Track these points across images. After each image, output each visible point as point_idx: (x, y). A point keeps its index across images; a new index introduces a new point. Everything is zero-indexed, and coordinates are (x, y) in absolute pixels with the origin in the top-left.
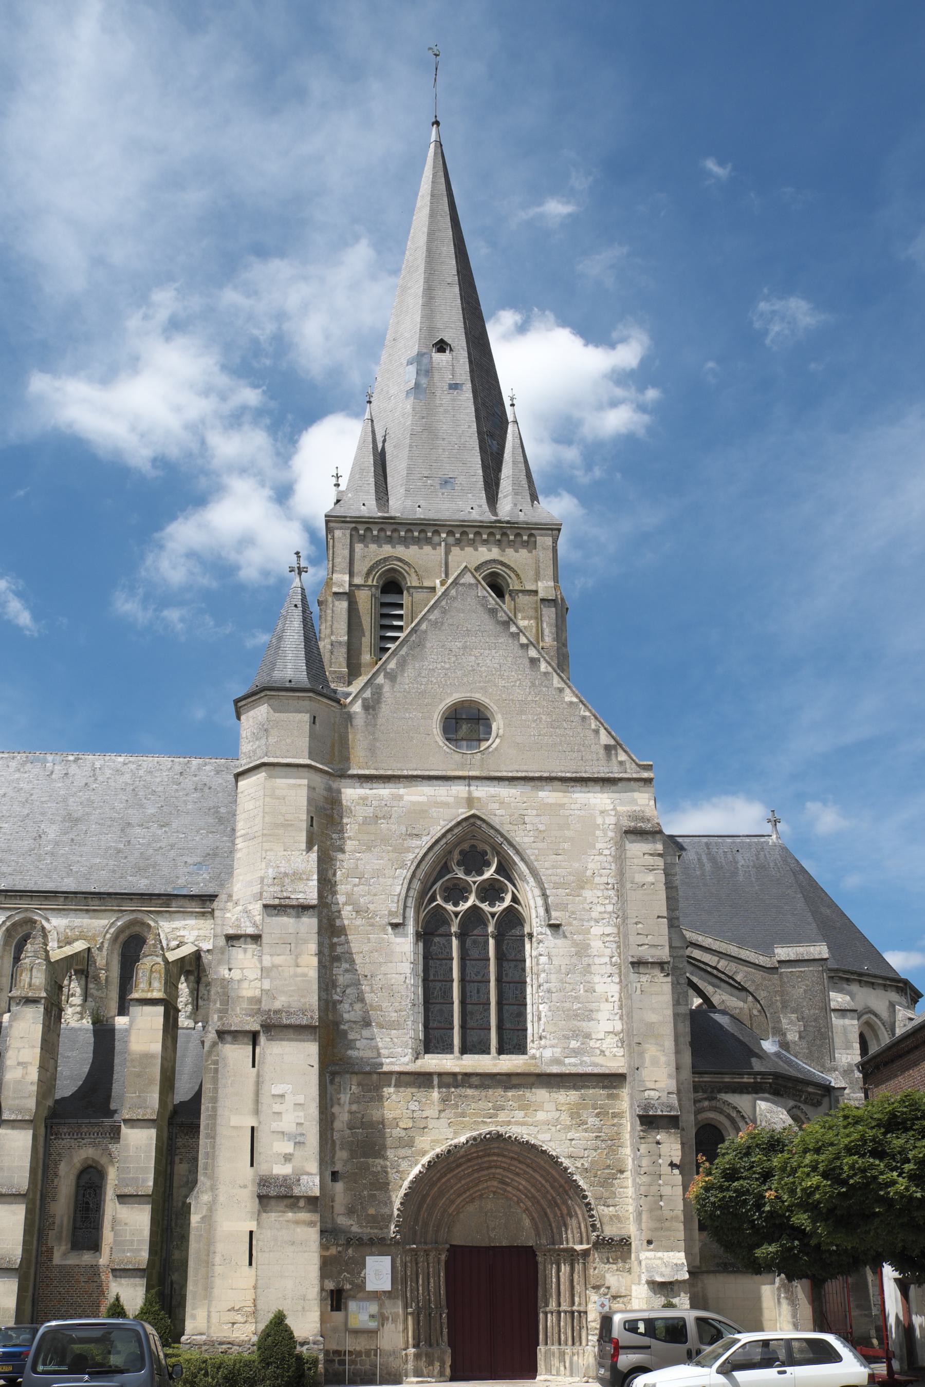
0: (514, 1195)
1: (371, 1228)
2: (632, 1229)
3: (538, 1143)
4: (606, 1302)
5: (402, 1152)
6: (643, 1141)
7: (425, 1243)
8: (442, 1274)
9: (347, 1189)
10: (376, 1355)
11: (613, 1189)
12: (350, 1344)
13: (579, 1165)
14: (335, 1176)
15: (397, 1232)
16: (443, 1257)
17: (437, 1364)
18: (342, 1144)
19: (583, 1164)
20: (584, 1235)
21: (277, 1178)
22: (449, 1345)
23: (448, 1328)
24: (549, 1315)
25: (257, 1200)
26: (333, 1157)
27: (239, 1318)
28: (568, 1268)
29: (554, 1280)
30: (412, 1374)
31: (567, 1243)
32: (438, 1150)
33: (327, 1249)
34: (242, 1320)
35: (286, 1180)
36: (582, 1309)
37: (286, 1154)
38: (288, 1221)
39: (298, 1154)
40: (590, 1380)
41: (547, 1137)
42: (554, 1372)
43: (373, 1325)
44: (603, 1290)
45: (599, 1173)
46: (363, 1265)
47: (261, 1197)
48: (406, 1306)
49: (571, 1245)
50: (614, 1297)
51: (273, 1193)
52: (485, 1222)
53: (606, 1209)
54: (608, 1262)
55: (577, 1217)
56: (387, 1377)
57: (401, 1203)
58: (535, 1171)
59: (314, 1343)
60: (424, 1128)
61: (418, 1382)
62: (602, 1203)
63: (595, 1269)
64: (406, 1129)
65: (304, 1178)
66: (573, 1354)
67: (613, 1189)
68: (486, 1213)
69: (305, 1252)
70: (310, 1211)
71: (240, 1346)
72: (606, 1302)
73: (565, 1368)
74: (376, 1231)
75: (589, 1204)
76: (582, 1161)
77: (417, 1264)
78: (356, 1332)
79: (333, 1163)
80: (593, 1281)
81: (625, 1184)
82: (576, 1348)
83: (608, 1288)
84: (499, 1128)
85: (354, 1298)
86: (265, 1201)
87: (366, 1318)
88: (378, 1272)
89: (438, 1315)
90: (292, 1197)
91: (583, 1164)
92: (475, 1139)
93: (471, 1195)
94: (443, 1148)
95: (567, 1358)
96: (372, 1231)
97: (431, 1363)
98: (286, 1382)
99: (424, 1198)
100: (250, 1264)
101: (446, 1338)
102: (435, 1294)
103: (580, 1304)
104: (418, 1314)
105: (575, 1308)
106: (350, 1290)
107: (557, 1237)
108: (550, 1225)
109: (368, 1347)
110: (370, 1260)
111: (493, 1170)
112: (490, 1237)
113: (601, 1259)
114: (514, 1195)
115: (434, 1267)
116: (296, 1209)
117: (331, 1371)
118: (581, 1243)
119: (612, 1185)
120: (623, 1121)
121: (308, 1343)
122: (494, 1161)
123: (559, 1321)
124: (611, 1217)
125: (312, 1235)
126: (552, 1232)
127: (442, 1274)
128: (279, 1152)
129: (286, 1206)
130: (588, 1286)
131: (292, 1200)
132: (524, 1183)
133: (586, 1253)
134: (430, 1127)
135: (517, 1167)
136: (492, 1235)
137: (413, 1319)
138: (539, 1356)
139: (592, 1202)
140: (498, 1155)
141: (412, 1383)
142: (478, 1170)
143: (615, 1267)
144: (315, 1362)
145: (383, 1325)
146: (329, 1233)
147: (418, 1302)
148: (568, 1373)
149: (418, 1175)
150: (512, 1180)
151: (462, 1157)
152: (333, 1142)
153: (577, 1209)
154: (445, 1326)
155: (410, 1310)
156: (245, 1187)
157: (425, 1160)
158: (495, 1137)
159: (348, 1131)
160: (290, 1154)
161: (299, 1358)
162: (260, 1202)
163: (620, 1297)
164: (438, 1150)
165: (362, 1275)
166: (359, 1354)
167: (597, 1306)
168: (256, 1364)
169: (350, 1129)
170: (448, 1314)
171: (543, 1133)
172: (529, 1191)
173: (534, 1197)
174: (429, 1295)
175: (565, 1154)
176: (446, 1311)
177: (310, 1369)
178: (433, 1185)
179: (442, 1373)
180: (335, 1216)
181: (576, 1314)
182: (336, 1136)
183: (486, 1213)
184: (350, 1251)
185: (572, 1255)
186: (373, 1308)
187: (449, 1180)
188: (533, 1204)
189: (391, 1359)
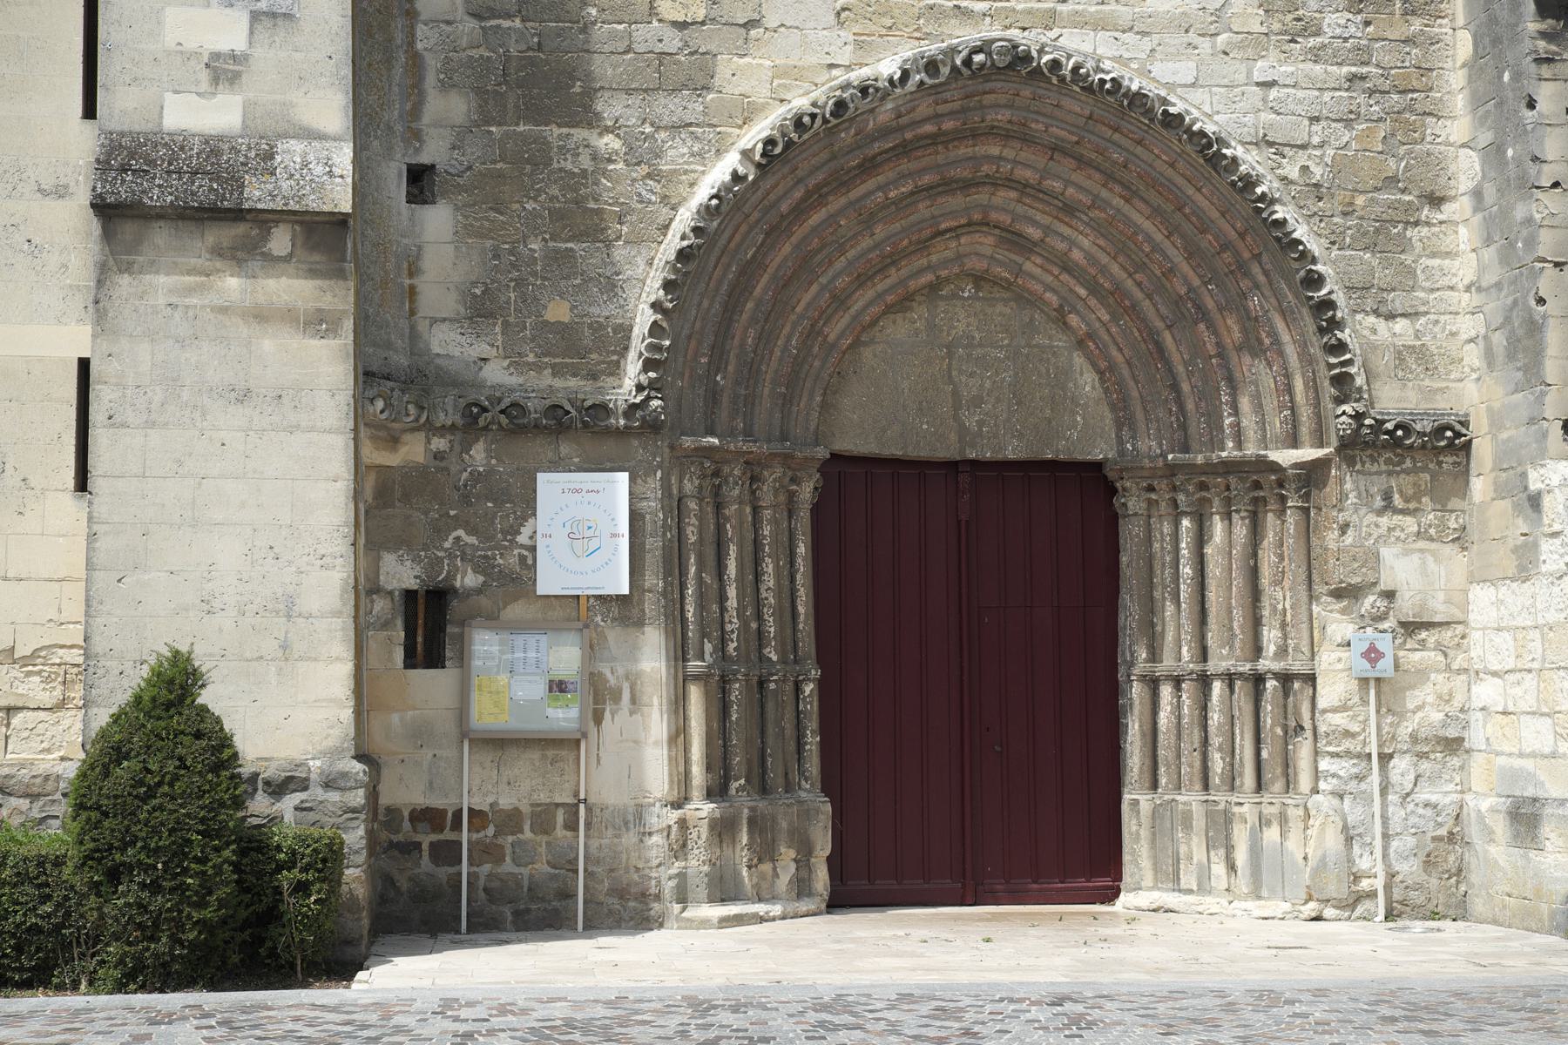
0: (1048, 288)
1: (557, 371)
2: (1472, 391)
3: (1152, 89)
4: (1385, 644)
5: (670, 107)
6: (1546, 71)
7: (748, 433)
8: (802, 549)
9: (466, 231)
10: (572, 826)
11: (1408, 258)
12: (477, 786)
13: (1293, 172)
14: (420, 182)
15: (652, 385)
16: (806, 492)
17: (787, 854)
18: (448, 68)
19: (1305, 169)
20: (1305, 414)
21: (177, 144)
22: (826, 789)
23: (823, 730)
24: (1166, 691)
25: (95, 226)
26: (416, 112)
27: (35, 690)
28: (1241, 531)
29: (1187, 571)
30: (703, 892)
31: (1239, 445)
32: (800, 103)
33: (393, 441)
34: (48, 697)
35: (215, 152)
36: (1297, 665)
37: (216, 56)
38: (224, 310)
39: (268, 57)
40: (1329, 912)
41: (1184, 71)
42: (1188, 880)
43: (564, 716)
44: (1369, 602)
45: (1360, 200)
46: (529, 506)
47: (106, 210)
48: (680, 652)
49: (1251, 450)
50: (1410, 628)
51: (157, 195)
52: (958, 379)
53: (1381, 325)
54: (1388, 507)
55: (1281, 353)
56: (614, 903)
57: (668, 286)
58: (1131, 194)
59: (328, 785)
60: (750, 24)
61: (726, 922)
62: (1370, 304)
63: (1344, 528)
64: (682, 26)
65: (291, 152)
66: (1263, 822)
67: (1408, 258)
68: (951, 348)
69: (292, 429)
70: (313, 273)
71: (33, 797)
72: (1385, 644)
73: (1232, 867)
74: (573, 383)
75: (1328, 304)
76: (1302, 158)
77: (719, 507)
78: (499, 744)
79: (415, 136)
80: (1340, 574)
81: (1447, 243)
82: (1271, 803)
83: (1390, 595)
84: (1014, 33)
85: (492, 620)
86: (128, 229)
87: (538, 689)
88: (586, 525)
89: (789, 687)
90: (238, 214)
91: (1305, 169)
92: (932, 66)
93: (902, 282)
94: (819, 94)
95: (1241, 837)
96: (558, 383)
97: (765, 852)
98: (193, 945)
99: (750, 271)
100: (82, 483)
101: (813, 765)
102: (778, 612)
103: (1282, 651)
104: (724, 682)
105: (1265, 664)
106: (479, 591)
107: (1197, 426)
108: (1175, 387)
109: (543, 797)
110: (550, 486)
111: (981, 196)
112: (962, 425)
113: (1365, 497)
114: (1048, 288)
115: (775, 522)
116: (255, 265)
117: (404, 885)
118: (1294, 442)
119: (1404, 246)
120: (1442, 28)
121: (303, 785)
122: (989, 159)
123: (1204, 709)
124: (1399, 356)
125: (323, 369)
126: (1182, 408)
127: (802, 549)
128: (191, 45)
129: (217, 252)
130: (1320, 589)
131: (240, 229)
132: (1086, 243)
133: (1312, 475)
134: (771, 21)
135: (1067, 183)
136: (971, 422)
137: (707, 696)
138: (1129, 825)
139: (1340, 298)
140: (1006, 136)
141: (704, 924)
142: (929, 191)
143: (1410, 524)
144: (329, 858)
145: (598, 719)
146: (391, 383)
147: (723, 641)
148: (1243, 883)
149: (726, 188)
150: (1047, 230)
151: (884, 132)
152: (416, 62)
153: (1280, 325)
154: (812, 725)
155: (695, 665)
156: (61, 192)
157: (753, 136)
158: (1001, 61)
159: (472, 24)
160: (233, 57)
161: (255, 846)
162: (108, 235)
163: (1429, 625)
164: (801, 103)
165: (523, 539)
166: (511, 821)
167: (1354, 658)
168: (67, 871)
169: (477, 16)
170: (822, 684)
171: (1168, 57)
172: (1104, 270)
173: (1118, 291)
174: (759, 616)
175: (1247, 133)
176: (815, 673)
177: (302, 888)
178: (776, 232)
179: (802, 888)
180: (422, 326)
181: (1271, 684)
182: (425, 38)
183: (951, 348)
184: (478, 453)
185: (1257, 485)
186: (566, 657)
187: (832, 219)
188: (1115, 318)
189: (630, 839)
